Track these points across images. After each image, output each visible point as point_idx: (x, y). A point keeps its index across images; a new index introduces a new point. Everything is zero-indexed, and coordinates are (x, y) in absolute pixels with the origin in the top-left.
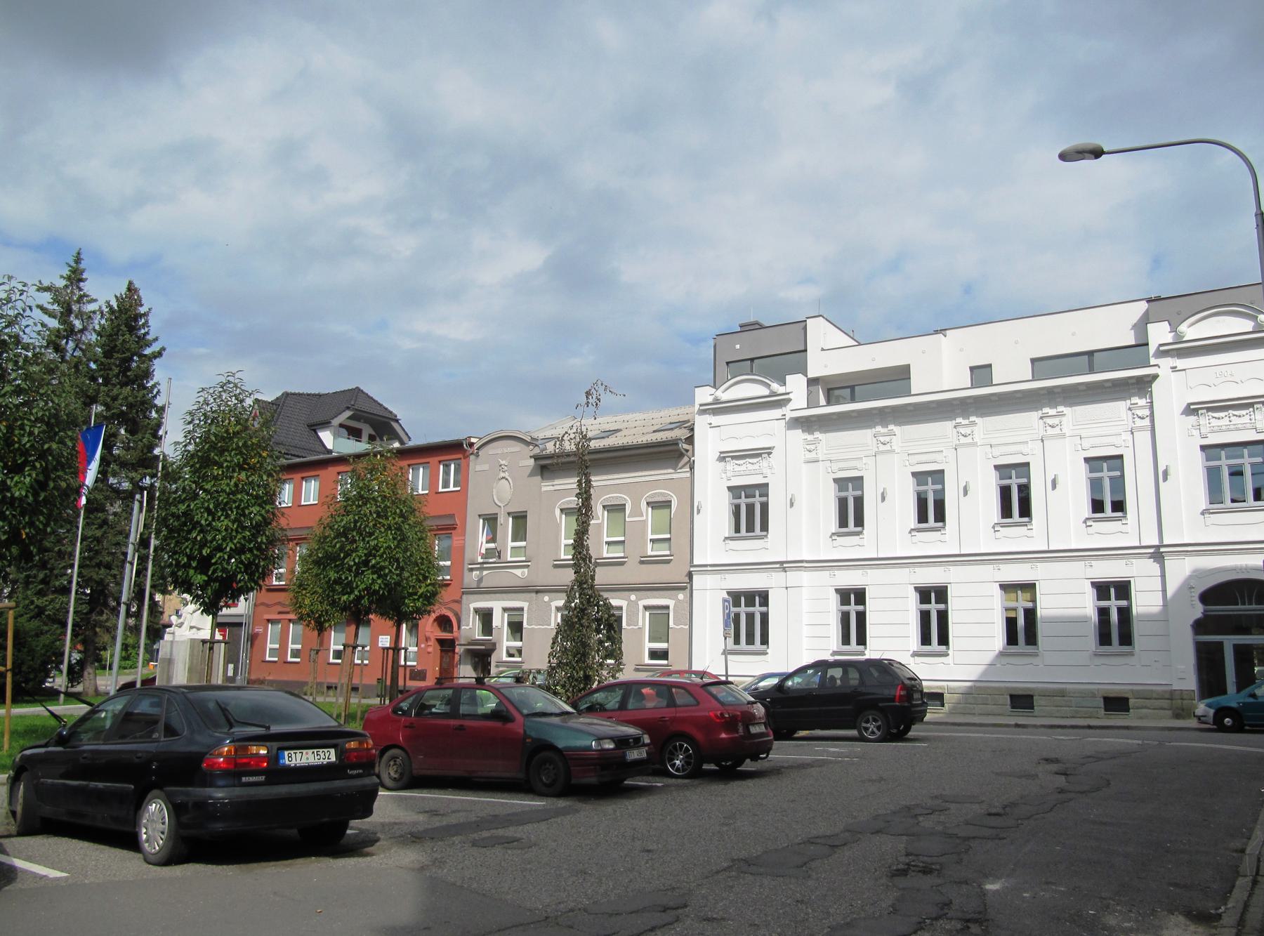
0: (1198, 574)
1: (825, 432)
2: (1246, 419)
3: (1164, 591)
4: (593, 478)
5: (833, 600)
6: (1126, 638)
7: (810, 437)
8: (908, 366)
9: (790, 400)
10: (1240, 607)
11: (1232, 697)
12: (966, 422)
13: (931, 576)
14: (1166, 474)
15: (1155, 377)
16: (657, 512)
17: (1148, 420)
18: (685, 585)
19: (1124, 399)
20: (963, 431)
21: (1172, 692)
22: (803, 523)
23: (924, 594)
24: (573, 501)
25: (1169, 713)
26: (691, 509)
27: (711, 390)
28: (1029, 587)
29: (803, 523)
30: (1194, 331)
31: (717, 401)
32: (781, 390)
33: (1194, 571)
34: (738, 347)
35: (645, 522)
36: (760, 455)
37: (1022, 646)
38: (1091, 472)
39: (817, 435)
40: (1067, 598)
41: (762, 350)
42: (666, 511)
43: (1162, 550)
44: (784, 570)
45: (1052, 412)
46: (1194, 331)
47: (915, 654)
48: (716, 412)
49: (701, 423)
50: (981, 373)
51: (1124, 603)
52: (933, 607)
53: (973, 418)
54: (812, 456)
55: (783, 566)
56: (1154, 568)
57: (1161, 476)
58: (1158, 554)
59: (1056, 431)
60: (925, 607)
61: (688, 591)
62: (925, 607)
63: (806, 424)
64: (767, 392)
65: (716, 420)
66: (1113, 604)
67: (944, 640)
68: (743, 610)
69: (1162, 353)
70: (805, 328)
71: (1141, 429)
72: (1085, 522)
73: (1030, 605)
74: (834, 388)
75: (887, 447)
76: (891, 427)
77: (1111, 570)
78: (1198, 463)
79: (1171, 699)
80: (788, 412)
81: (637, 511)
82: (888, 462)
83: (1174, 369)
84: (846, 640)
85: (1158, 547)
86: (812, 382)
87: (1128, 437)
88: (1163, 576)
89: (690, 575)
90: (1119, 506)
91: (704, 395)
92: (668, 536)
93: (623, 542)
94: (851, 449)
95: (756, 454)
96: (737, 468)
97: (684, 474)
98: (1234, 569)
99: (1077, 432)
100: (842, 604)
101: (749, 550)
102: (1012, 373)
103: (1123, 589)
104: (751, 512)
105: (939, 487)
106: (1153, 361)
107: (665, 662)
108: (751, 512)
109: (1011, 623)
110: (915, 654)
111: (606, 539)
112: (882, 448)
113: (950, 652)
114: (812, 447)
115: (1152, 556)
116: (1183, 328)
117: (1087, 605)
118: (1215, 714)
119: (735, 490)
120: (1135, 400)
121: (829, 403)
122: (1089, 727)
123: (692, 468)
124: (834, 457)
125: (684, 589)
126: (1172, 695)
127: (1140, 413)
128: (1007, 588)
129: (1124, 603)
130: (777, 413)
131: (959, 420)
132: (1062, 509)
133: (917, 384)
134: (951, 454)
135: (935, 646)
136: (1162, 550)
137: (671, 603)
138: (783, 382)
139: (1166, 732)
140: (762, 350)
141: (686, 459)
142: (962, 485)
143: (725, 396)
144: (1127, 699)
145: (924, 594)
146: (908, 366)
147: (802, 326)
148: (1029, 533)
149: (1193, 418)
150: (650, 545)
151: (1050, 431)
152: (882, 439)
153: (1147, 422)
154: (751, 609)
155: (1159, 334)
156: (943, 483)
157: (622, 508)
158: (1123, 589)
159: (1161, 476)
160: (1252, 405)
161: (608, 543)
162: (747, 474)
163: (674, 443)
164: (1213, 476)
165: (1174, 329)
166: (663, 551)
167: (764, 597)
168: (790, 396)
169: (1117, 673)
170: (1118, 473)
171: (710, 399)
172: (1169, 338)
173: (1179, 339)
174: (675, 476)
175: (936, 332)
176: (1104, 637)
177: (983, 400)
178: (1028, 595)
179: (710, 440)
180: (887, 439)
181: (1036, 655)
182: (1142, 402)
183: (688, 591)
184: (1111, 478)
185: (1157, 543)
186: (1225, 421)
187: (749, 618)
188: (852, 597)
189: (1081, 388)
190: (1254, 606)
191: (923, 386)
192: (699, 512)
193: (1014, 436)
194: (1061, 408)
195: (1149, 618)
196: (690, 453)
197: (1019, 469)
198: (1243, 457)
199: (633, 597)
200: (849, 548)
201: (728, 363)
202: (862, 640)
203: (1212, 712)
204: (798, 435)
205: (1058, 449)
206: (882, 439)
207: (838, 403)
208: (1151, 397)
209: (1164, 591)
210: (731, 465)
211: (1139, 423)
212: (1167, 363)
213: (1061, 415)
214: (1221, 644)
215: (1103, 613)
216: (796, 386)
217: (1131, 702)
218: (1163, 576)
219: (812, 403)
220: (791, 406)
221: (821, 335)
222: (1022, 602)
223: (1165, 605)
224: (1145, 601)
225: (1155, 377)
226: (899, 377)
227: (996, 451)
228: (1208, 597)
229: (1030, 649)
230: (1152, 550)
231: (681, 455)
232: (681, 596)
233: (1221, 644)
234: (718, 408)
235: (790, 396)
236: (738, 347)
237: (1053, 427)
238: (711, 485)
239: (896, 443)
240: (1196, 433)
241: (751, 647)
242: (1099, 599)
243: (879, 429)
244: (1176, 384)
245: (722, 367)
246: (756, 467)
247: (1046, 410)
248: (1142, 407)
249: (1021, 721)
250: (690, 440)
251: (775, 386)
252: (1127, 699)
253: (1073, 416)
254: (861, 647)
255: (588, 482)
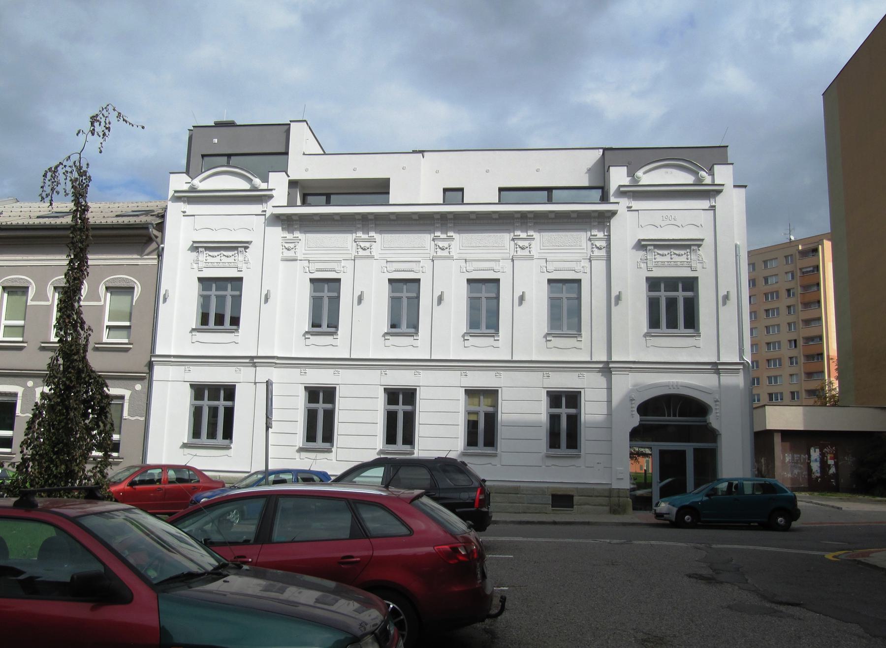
0: (638, 389)
1: (306, 232)
2: (683, 258)
3: (609, 401)
4: (89, 257)
5: (187, 394)
6: (573, 441)
7: (289, 236)
8: (388, 179)
9: (271, 197)
10: (666, 418)
11: (694, 495)
12: (444, 236)
13: (401, 379)
14: (618, 298)
15: (614, 213)
16: (116, 297)
17: (604, 250)
18: (146, 376)
19: (585, 230)
20: (441, 244)
21: (611, 490)
22: (275, 319)
23: (392, 395)
24: (60, 279)
25: (607, 508)
26: (155, 296)
27: (185, 178)
28: (492, 394)
29: (275, 319)
30: (649, 178)
31: (193, 189)
32: (264, 186)
33: (634, 386)
34: (216, 141)
35: (102, 308)
36: (236, 248)
37: (563, 450)
38: (203, 290)
39: (297, 234)
40: (524, 406)
41: (240, 148)
42: (128, 298)
43: (255, 361)
44: (254, 365)
45: (523, 235)
46: (649, 178)
47: (301, 450)
48: (190, 200)
49: (174, 211)
50: (453, 193)
51: (572, 411)
52: (321, 407)
53: (450, 234)
54: (290, 254)
55: (253, 361)
56: (601, 381)
57: (613, 300)
58: (607, 369)
59: (526, 252)
60: (393, 408)
61: (146, 381)
62: (393, 408)
63: (286, 222)
64: (247, 186)
65: (191, 209)
66: (564, 411)
67: (328, 437)
68: (206, 404)
69: (622, 193)
70: (288, 132)
71: (598, 258)
72: (304, 335)
73: (491, 409)
74: (305, 190)
75: (367, 253)
76: (372, 234)
77: (565, 382)
78: (194, 290)
79: (609, 497)
80: (270, 208)
81: (41, 295)
82: (366, 266)
83: (629, 208)
84: (391, 438)
85: (607, 363)
86: (293, 184)
87: (586, 263)
88: (609, 389)
89: (150, 365)
90: (235, 321)
91: (179, 182)
92: (127, 324)
93: (129, 327)
94: (330, 251)
95: (689, 245)
96: (210, 259)
97: (150, 261)
98: (667, 386)
99: (464, 256)
100: (196, 398)
101: (217, 343)
102: (481, 196)
103: (573, 398)
104: (220, 306)
105: (237, 293)
106: (612, 199)
107: (8, 450)
108: (220, 306)
109: (472, 426)
110: (301, 450)
111: (107, 323)
112: (361, 252)
113: (334, 449)
114: (292, 245)
115: (601, 370)
116: (640, 173)
117: (541, 412)
118: (678, 512)
119: (204, 282)
120: (594, 232)
121: (304, 203)
122: (555, 523)
123: (160, 255)
124: (468, 257)
125: (141, 379)
126: (610, 493)
127: (598, 244)
128: (471, 393)
129: (572, 411)
130: (257, 208)
131: (438, 234)
132: (525, 324)
133: (395, 196)
134: (428, 264)
135: (319, 443)
136: (255, 361)
137: (127, 393)
138: (265, 180)
139: (517, 526)
140: (240, 148)
141: (154, 246)
142: (264, 292)
143: (202, 186)
144: (573, 496)
145: (392, 395)
146: (388, 179)
147: (286, 129)
148: (495, 344)
149: (641, 253)
150: (105, 332)
151: (520, 252)
152: (363, 244)
153: (603, 253)
154: (215, 403)
155: (618, 177)
156: (240, 290)
157: (24, 290)
158: (573, 398)
159: (613, 300)
160: (689, 246)
161: (108, 327)
162: (220, 267)
163: (145, 227)
164: (653, 305)
165: (631, 174)
166: (121, 339)
167: (229, 392)
168: (273, 193)
169: (565, 474)
170: (335, 294)
171: (186, 187)
172: (626, 181)
173: (635, 182)
174: (140, 262)
175: (414, 152)
176: (554, 440)
177: (451, 218)
178: (489, 401)
179: (182, 228)
180: (367, 245)
181: (495, 455)
182: (600, 235)
183: (146, 381)
184: (330, 298)
185: (604, 359)
186: (217, 259)
187: (214, 410)
188: (222, 393)
189: (393, 217)
190: (677, 418)
191: (404, 196)
192: (165, 300)
193: (487, 252)
194: (531, 233)
195: (596, 426)
196: (159, 240)
197: (331, 284)
198: (226, 290)
199: (30, 383)
200: (402, 348)
201: (203, 156)
202: (409, 439)
203: (675, 510)
204: (277, 233)
205: (528, 266)
206: (363, 244)
207: (310, 205)
208: (609, 231)
209: (609, 401)
210: (203, 256)
211: (597, 253)
212: (624, 202)
213: (531, 238)
214: (683, 453)
215: (554, 419)
216: (278, 184)
217: (576, 499)
218: (609, 389)
219: (291, 203)
220: (272, 203)
221: (301, 140)
222: (484, 407)
223: (610, 414)
224: (592, 410)
225: (614, 213)
226: (379, 188)
227: (314, 266)
228: (645, 408)
229: (489, 450)
230: (601, 366)
231: (149, 240)
232: (138, 387)
233: (683, 453)
234: (193, 197)
235: (273, 193)
236: (216, 141)
237: (288, 250)
238: (180, 277)
239: (376, 249)
240: (643, 265)
241: (212, 442)
242: (551, 407)
243: (360, 234)
244: (632, 222)
245: (196, 160)
246: (231, 260)
247: (517, 233)
248: (600, 239)
249: (558, 519)
250: (161, 227)
251: (257, 181)
252: (573, 496)
253: (540, 241)
254: (227, 441)
255: (83, 261)
